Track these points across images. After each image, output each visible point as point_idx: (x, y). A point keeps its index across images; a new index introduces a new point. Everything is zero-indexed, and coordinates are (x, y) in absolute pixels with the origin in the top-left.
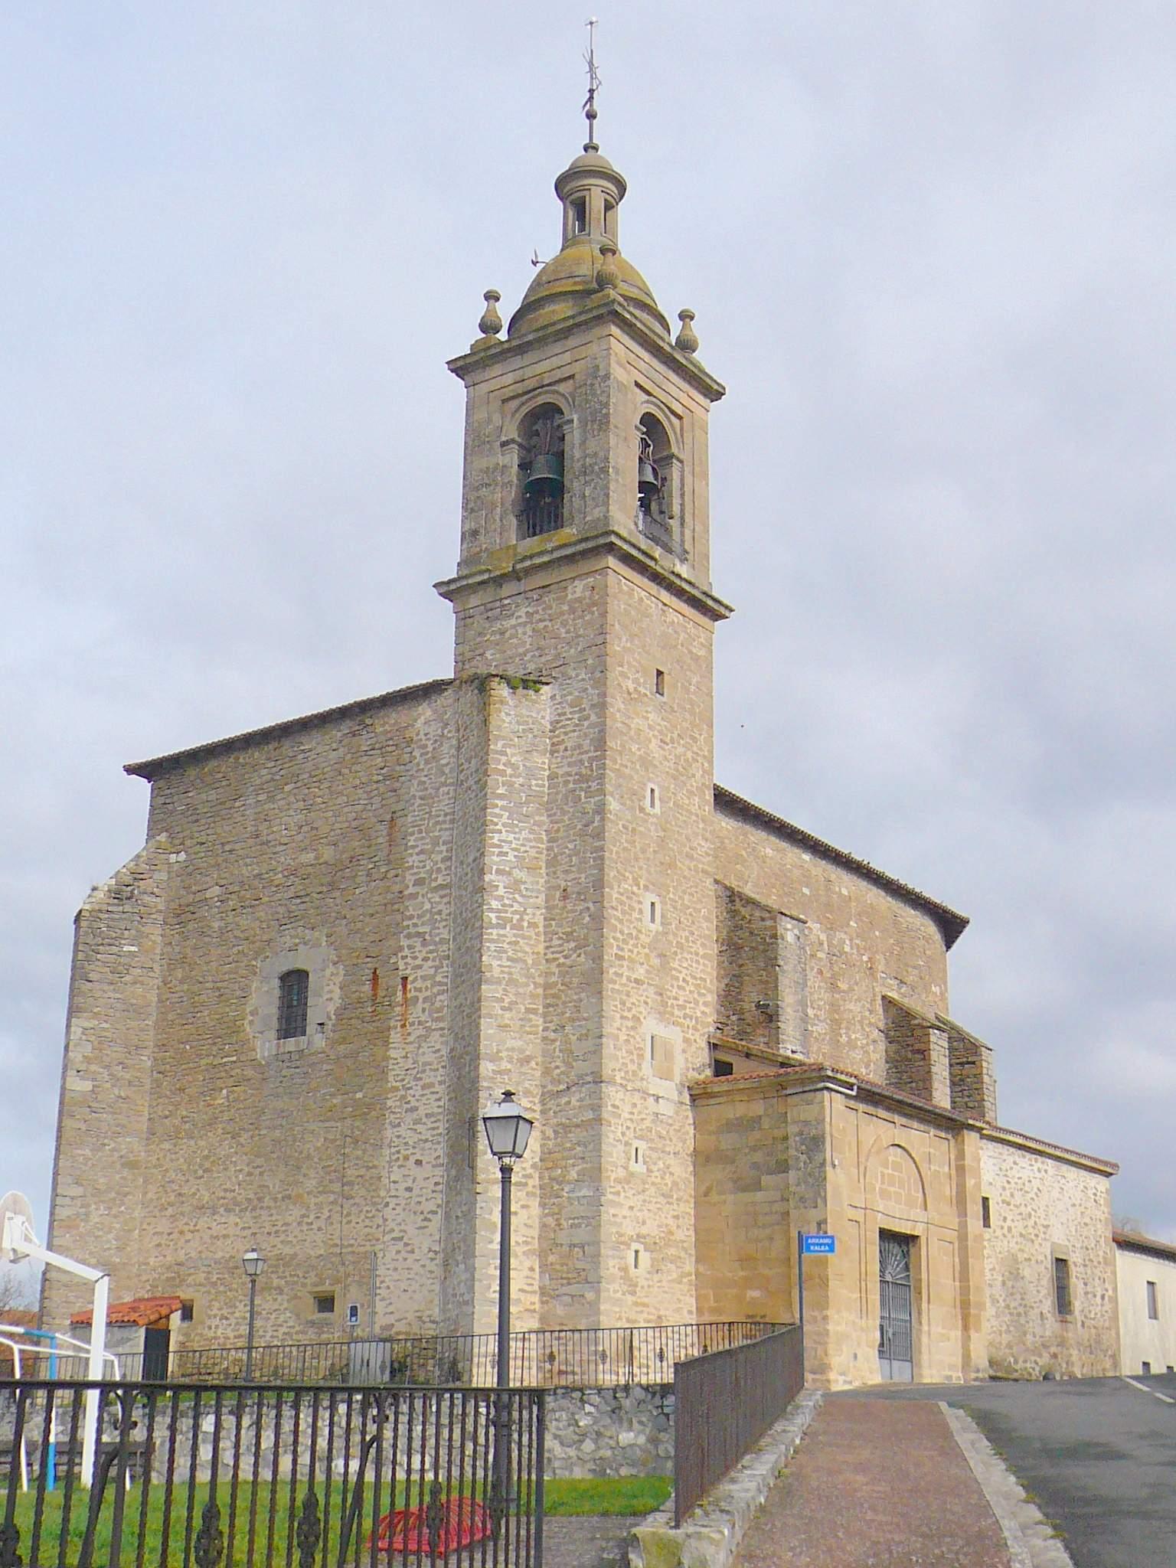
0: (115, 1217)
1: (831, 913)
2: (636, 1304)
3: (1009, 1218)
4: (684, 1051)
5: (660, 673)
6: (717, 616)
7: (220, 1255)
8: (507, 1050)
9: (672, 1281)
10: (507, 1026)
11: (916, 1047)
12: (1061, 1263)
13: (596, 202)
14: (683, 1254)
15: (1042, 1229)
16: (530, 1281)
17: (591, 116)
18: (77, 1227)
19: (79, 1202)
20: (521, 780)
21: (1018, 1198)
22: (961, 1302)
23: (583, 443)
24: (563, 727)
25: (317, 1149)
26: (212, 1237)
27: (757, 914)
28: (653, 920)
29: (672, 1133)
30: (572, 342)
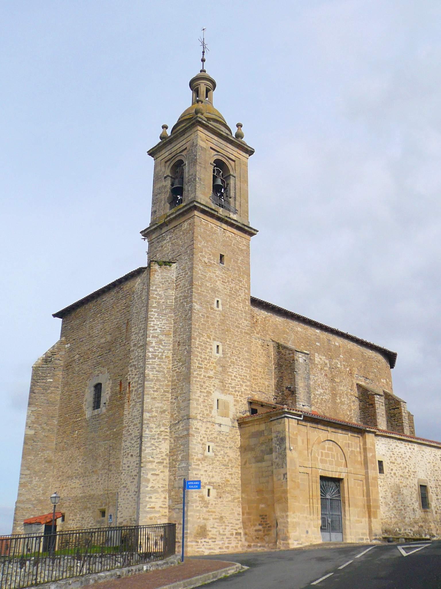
0: (42, 481)
1: (330, 352)
2: (209, 512)
3: (394, 469)
4: (235, 405)
5: (222, 256)
6: (252, 234)
7: (73, 495)
8: (156, 408)
9: (229, 501)
10: (155, 398)
12: (423, 488)
13: (203, 89)
14: (234, 490)
15: (412, 473)
16: (164, 503)
17: (203, 60)
18: (27, 486)
19: (28, 476)
20: (163, 301)
21: (399, 460)
22: (367, 505)
23: (189, 172)
24: (180, 278)
25: (102, 452)
26: (71, 488)
27: (287, 352)
28: (218, 352)
29: (228, 439)
30: (186, 136)
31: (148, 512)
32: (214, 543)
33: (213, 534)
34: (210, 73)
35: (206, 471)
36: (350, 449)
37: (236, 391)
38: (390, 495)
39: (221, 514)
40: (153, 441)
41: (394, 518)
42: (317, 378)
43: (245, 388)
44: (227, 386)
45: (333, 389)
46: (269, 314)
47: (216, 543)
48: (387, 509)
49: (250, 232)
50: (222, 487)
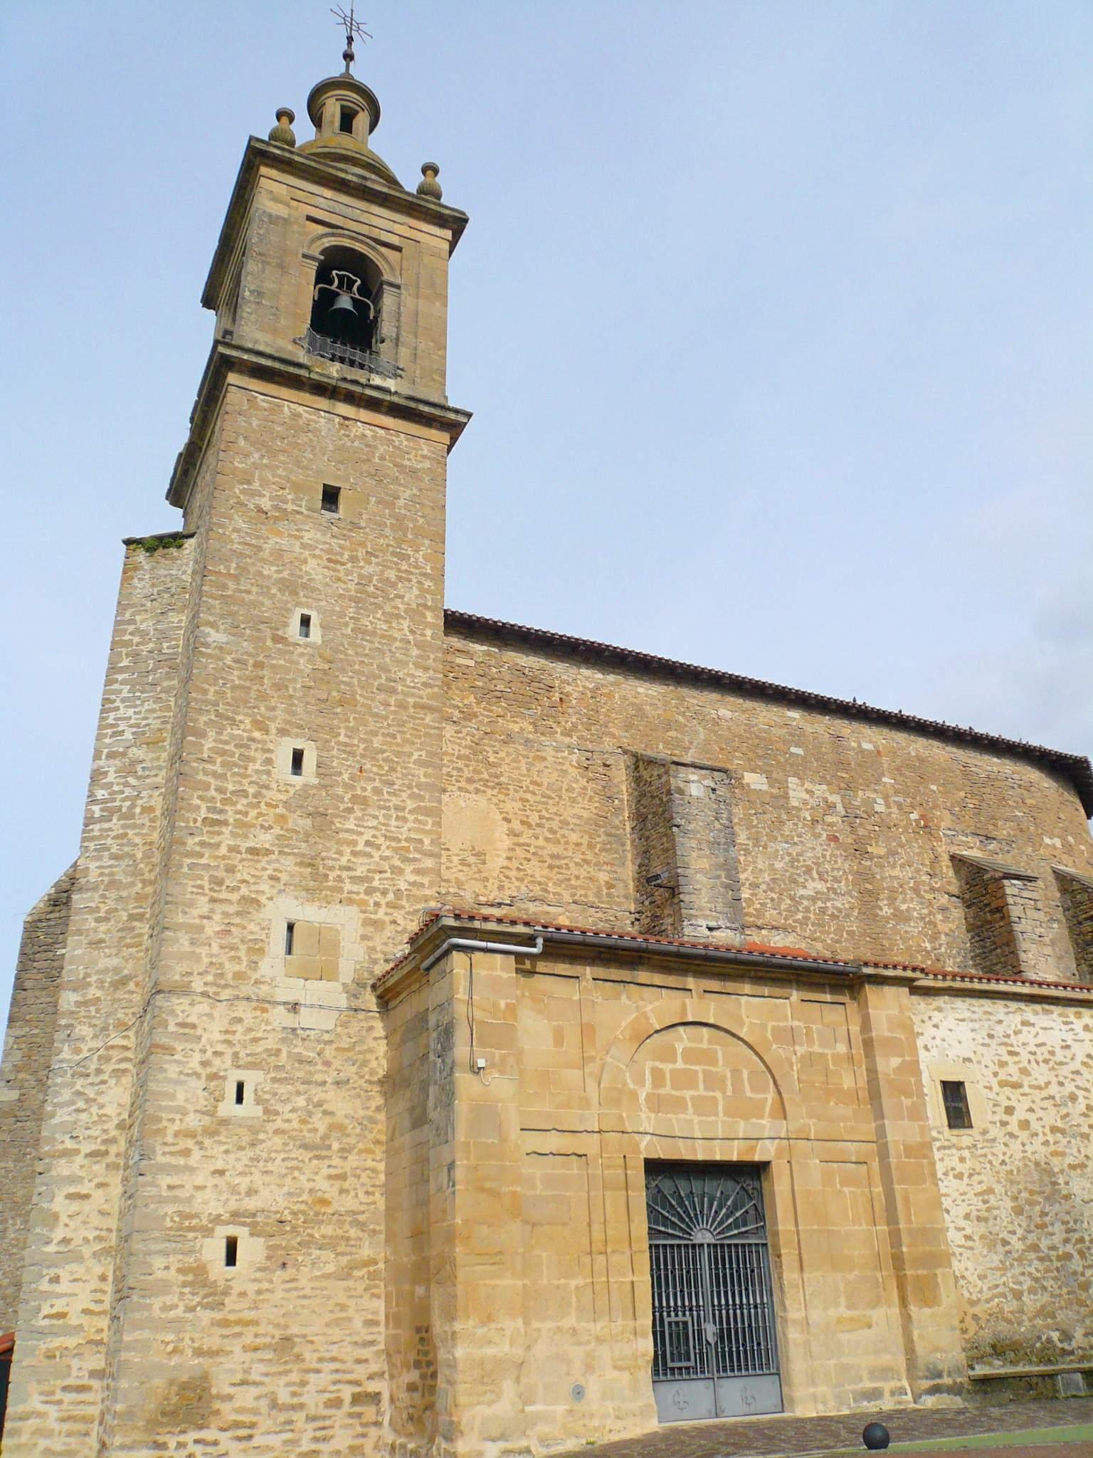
2: (224, 1323)
4: (364, 937)
8: (98, 972)
9: (326, 1276)
10: (101, 941)
11: (993, 905)
14: (353, 1233)
16: (99, 1296)
20: (151, 646)
31: (42, 1333)
32: (243, 1445)
33: (240, 1411)
34: (359, 73)
35: (221, 1173)
36: (801, 1050)
37: (370, 891)
38: (1009, 1204)
39: (287, 1327)
40: (79, 1084)
41: (1032, 1291)
42: (798, 849)
43: (412, 878)
44: (332, 875)
45: (863, 876)
46: (611, 678)
47: (256, 1441)
48: (995, 1259)
49: (451, 424)
50: (294, 1228)
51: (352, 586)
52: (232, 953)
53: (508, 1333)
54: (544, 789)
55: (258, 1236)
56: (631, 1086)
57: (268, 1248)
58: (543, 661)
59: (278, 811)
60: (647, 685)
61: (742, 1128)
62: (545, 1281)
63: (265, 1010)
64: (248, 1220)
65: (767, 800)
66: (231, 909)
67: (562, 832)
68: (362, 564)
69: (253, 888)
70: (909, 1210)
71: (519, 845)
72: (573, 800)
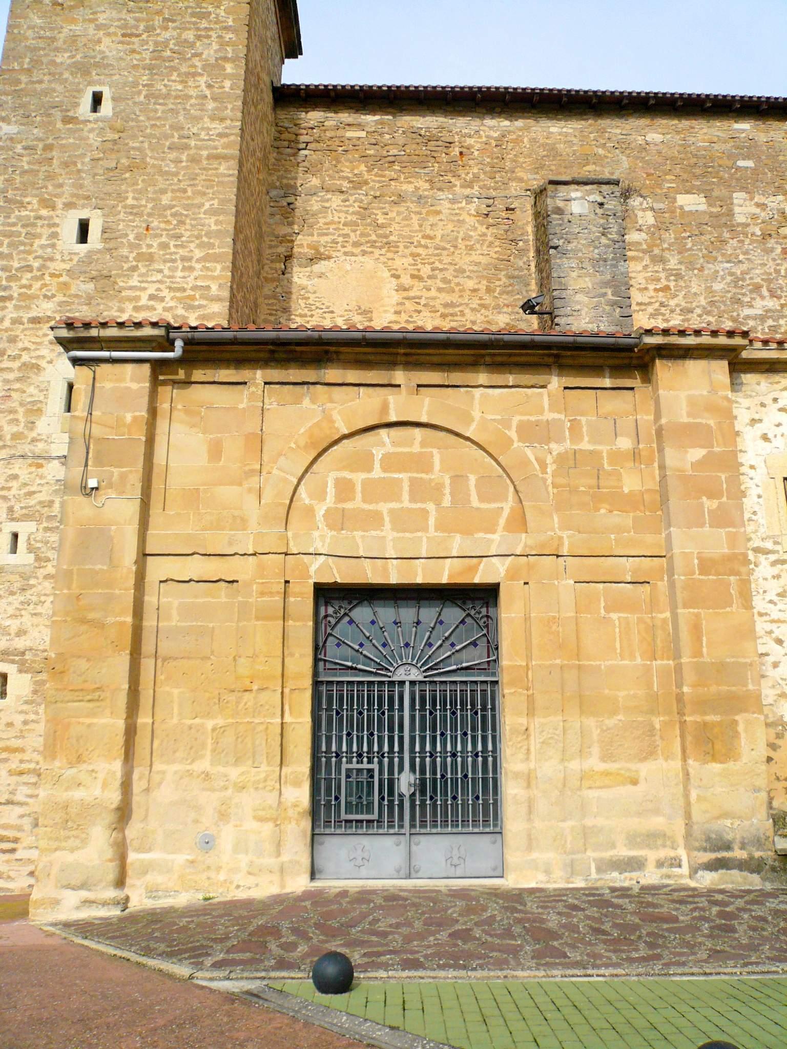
46: (520, 123)
47: (19, 855)
51: (147, 55)
52: (11, 416)
53: (101, 776)
54: (437, 241)
55: (26, 672)
56: (307, 502)
57: (36, 683)
58: (442, 119)
59: (61, 279)
60: (563, 123)
61: (457, 544)
62: (175, 721)
63: (40, 466)
64: (17, 658)
65: (706, 219)
66: (11, 376)
67: (457, 280)
68: (158, 31)
69: (34, 354)
70: (699, 639)
71: (408, 298)
72: (471, 248)
